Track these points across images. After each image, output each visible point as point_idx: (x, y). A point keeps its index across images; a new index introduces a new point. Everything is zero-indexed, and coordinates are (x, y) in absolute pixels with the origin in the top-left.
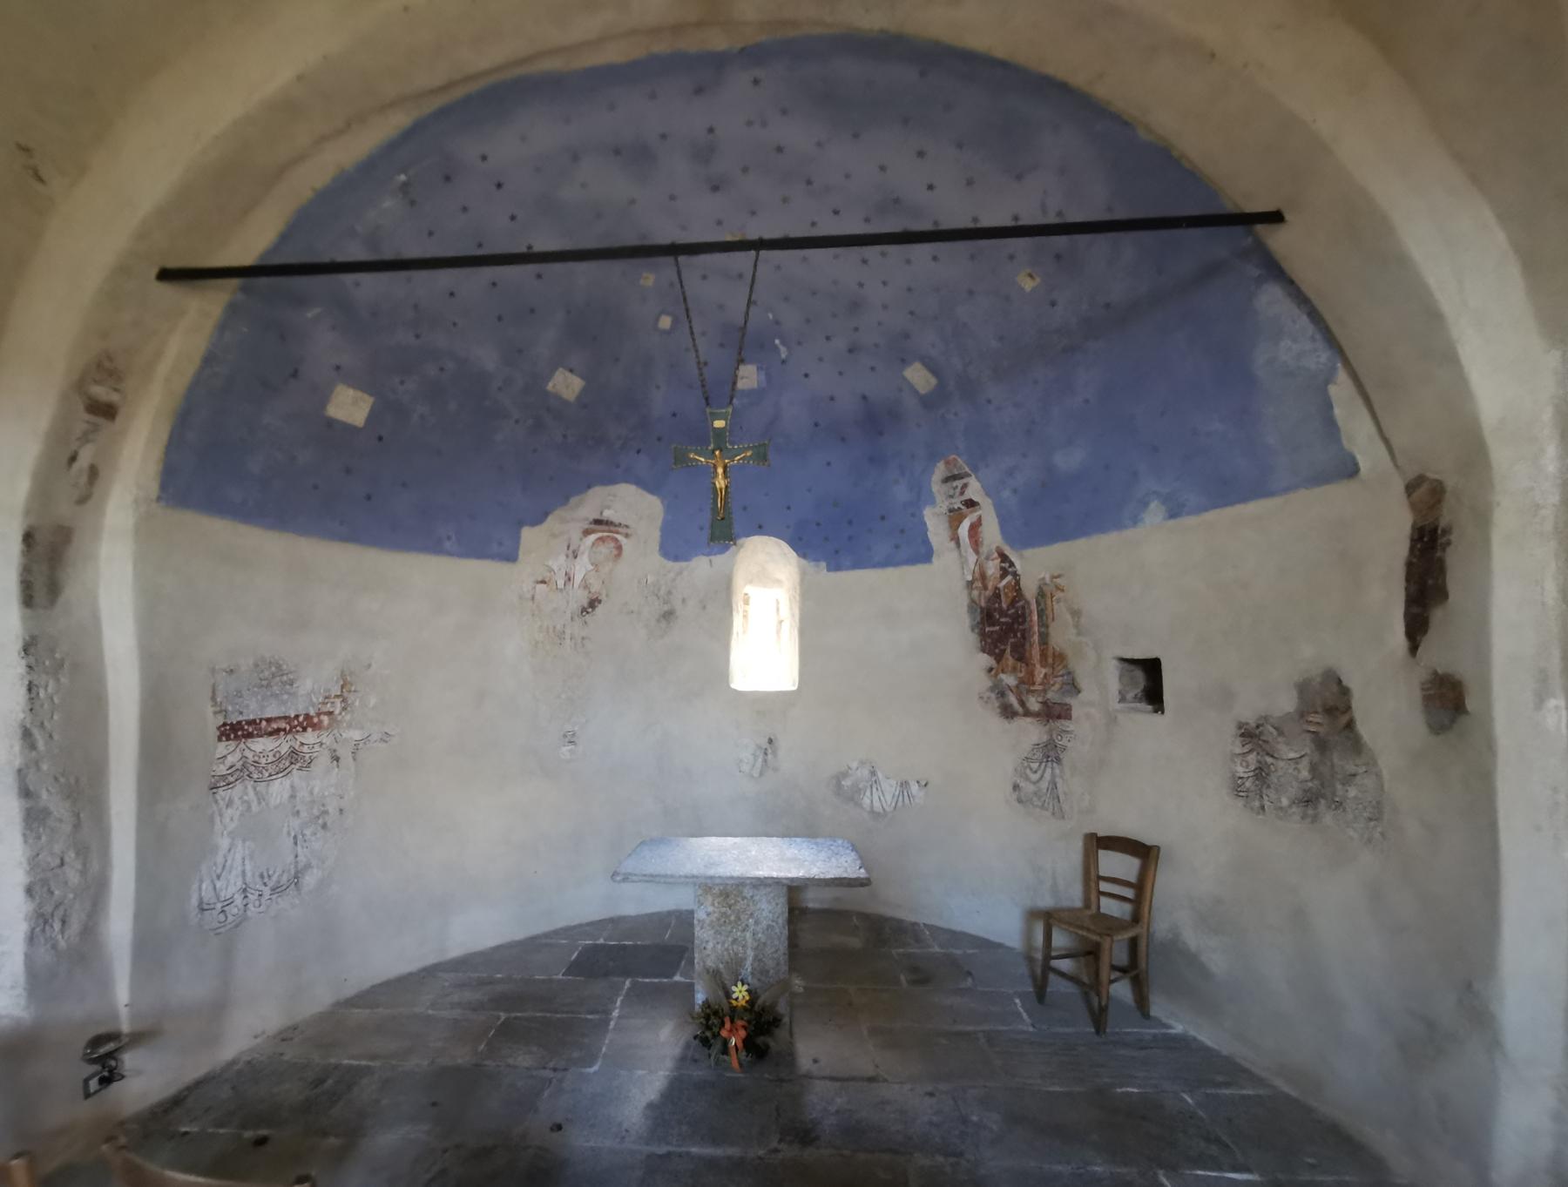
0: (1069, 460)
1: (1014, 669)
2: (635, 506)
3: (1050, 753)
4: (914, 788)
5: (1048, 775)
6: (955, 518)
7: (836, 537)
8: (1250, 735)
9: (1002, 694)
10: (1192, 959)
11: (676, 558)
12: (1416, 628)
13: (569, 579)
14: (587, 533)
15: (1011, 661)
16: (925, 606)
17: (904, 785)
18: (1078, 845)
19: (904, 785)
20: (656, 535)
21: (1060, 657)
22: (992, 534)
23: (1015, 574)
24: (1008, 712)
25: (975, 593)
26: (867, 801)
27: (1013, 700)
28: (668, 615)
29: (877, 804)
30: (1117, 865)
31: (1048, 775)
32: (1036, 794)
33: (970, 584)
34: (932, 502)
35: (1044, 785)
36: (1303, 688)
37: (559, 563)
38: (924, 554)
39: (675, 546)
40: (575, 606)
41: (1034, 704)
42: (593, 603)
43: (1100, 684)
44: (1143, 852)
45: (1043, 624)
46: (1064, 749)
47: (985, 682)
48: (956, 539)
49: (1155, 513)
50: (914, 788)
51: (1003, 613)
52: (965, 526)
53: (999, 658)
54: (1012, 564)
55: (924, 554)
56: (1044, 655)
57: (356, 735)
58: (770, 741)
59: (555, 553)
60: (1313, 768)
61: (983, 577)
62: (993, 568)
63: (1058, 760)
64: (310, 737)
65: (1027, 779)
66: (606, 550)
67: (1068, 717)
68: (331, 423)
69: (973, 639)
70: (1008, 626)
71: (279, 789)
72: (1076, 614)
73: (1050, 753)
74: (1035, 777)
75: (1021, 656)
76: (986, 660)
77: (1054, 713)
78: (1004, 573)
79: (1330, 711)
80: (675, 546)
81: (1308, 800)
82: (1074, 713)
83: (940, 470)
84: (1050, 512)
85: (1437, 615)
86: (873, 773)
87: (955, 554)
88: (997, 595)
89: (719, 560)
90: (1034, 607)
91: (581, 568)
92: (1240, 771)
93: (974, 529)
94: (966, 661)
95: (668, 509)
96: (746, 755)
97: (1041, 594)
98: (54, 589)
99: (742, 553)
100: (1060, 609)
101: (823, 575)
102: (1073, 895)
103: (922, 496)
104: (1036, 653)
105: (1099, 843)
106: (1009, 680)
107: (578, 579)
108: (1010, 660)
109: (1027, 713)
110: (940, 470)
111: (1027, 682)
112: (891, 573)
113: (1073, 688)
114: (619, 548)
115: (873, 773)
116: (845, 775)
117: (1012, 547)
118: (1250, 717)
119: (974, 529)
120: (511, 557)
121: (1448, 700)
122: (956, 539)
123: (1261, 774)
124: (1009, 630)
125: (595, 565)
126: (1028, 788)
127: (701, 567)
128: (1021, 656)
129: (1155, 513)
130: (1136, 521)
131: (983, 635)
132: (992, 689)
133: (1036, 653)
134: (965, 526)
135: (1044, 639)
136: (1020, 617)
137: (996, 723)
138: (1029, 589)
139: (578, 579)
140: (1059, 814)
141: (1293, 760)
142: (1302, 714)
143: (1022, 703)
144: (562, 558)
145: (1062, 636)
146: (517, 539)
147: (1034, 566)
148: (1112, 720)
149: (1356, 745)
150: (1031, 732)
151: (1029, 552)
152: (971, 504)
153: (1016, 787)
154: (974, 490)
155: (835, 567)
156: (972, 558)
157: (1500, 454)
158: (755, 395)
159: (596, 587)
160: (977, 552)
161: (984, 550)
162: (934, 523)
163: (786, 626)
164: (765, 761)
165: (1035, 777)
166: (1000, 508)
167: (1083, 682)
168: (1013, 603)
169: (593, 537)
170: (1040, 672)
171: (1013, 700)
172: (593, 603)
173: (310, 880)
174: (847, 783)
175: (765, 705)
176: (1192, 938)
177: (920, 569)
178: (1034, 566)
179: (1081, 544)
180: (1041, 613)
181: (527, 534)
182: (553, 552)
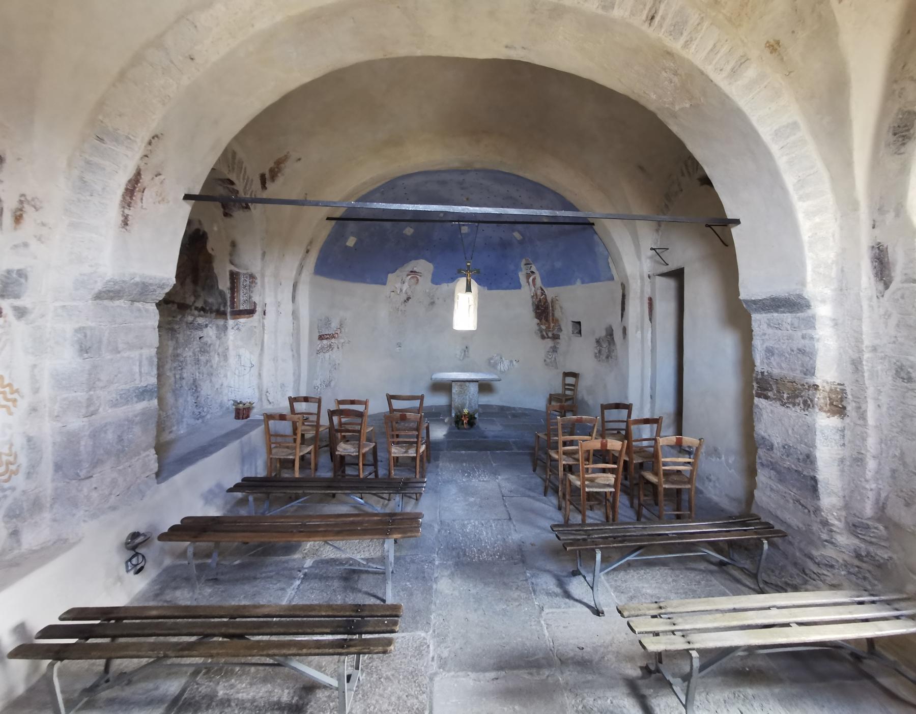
0: (558, 264)
2: (424, 267)
3: (554, 349)
7: (493, 278)
8: (598, 342)
9: (541, 332)
10: (586, 403)
13: (401, 290)
14: (408, 275)
16: (518, 302)
17: (511, 362)
18: (561, 375)
19: (511, 362)
20: (430, 276)
21: (557, 320)
24: (543, 337)
28: (433, 303)
30: (570, 380)
32: (551, 363)
34: (521, 270)
37: (398, 285)
38: (518, 286)
39: (437, 280)
40: (402, 300)
41: (550, 335)
42: (408, 299)
43: (567, 329)
44: (575, 375)
45: (553, 310)
47: (537, 328)
48: (528, 282)
49: (579, 282)
52: (531, 279)
57: (342, 341)
59: (399, 283)
62: (539, 292)
64: (333, 341)
66: (413, 281)
68: (347, 247)
69: (533, 314)
71: (327, 355)
72: (561, 308)
73: (554, 349)
75: (547, 320)
77: (556, 337)
78: (542, 294)
80: (437, 280)
81: (607, 357)
83: (524, 262)
84: (554, 278)
88: (540, 301)
91: (405, 287)
93: (534, 280)
95: (435, 267)
96: (458, 352)
97: (552, 301)
100: (557, 306)
101: (486, 291)
102: (559, 390)
103: (518, 268)
105: (566, 374)
106: (544, 327)
108: (544, 321)
110: (524, 262)
111: (548, 328)
112: (508, 291)
113: (560, 330)
116: (491, 359)
119: (534, 280)
120: (384, 284)
121: (625, 330)
122: (528, 282)
126: (548, 361)
127: (445, 287)
128: (547, 320)
129: (579, 282)
130: (575, 283)
131: (536, 313)
134: (531, 279)
135: (553, 315)
136: (547, 308)
137: (540, 340)
138: (549, 300)
140: (557, 368)
142: (606, 336)
145: (558, 314)
146: (386, 278)
147: (551, 293)
148: (570, 339)
150: (549, 343)
151: (550, 289)
152: (533, 272)
154: (534, 269)
155: (490, 288)
156: (533, 289)
157: (631, 281)
158: (467, 235)
159: (410, 293)
162: (522, 276)
163: (472, 307)
166: (541, 275)
167: (563, 328)
170: (552, 325)
172: (408, 299)
173: (333, 384)
175: (466, 336)
176: (586, 398)
177: (517, 291)
178: (551, 293)
179: (562, 288)
181: (390, 275)
182: (397, 283)
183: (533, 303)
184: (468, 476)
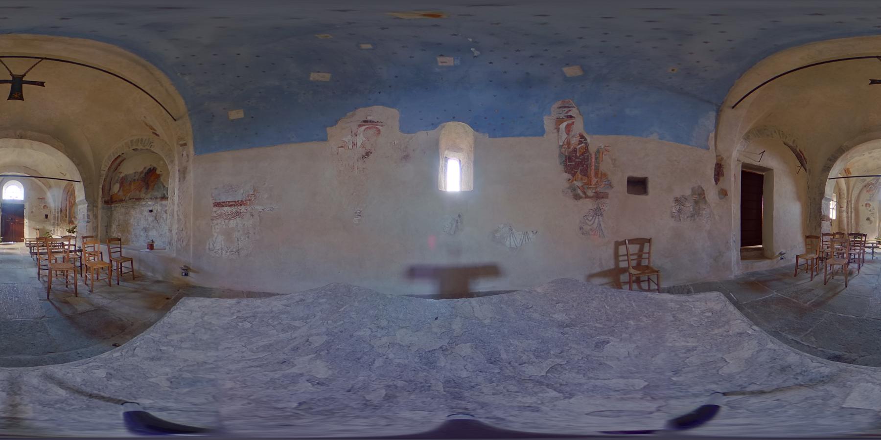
1: (582, 179)
4: (531, 235)
5: (597, 221)
6: (559, 121)
11: (409, 133)
12: (717, 180)
13: (354, 144)
14: (360, 126)
15: (580, 176)
16: (542, 155)
17: (526, 233)
18: (612, 245)
19: (526, 233)
22: (579, 127)
23: (586, 144)
25: (563, 150)
26: (508, 243)
27: (579, 192)
29: (513, 244)
31: (597, 221)
33: (561, 146)
35: (595, 225)
36: (693, 189)
37: (348, 138)
38: (541, 133)
39: (406, 127)
41: (590, 193)
46: (604, 210)
50: (531, 235)
51: (576, 157)
53: (574, 175)
54: (586, 139)
55: (541, 133)
56: (596, 174)
58: (459, 216)
60: (694, 208)
61: (569, 144)
62: (574, 141)
63: (602, 215)
65: (587, 224)
66: (371, 132)
67: (607, 198)
69: (561, 168)
70: (577, 162)
74: (590, 223)
75: (585, 173)
76: (567, 176)
78: (581, 142)
79: (700, 195)
80: (406, 127)
82: (609, 196)
85: (721, 178)
86: (511, 230)
87: (556, 134)
88: (575, 150)
89: (432, 133)
90: (593, 156)
91: (360, 140)
92: (674, 210)
94: (557, 176)
97: (598, 151)
98: (184, 178)
99: (443, 132)
101: (485, 138)
104: (593, 173)
105: (618, 244)
107: (359, 144)
109: (587, 197)
112: (522, 139)
114: (379, 131)
115: (511, 230)
117: (588, 133)
118: (678, 195)
120: (324, 139)
123: (680, 211)
124: (578, 165)
125: (368, 139)
127: (422, 136)
128: (585, 173)
131: (566, 166)
132: (569, 188)
133: (593, 173)
135: (597, 169)
138: (592, 149)
139: (359, 144)
141: (689, 207)
143: (585, 193)
144: (350, 137)
147: (595, 142)
149: (706, 202)
150: (588, 205)
153: (581, 228)
154: (574, 112)
156: (564, 136)
160: (568, 134)
161: (572, 133)
162: (548, 123)
164: (457, 226)
165: (590, 223)
168: (582, 154)
169: (364, 128)
170: (594, 181)
171: (579, 192)
174: (498, 235)
180: (596, 159)
183: (561, 154)
184: (861, 261)
